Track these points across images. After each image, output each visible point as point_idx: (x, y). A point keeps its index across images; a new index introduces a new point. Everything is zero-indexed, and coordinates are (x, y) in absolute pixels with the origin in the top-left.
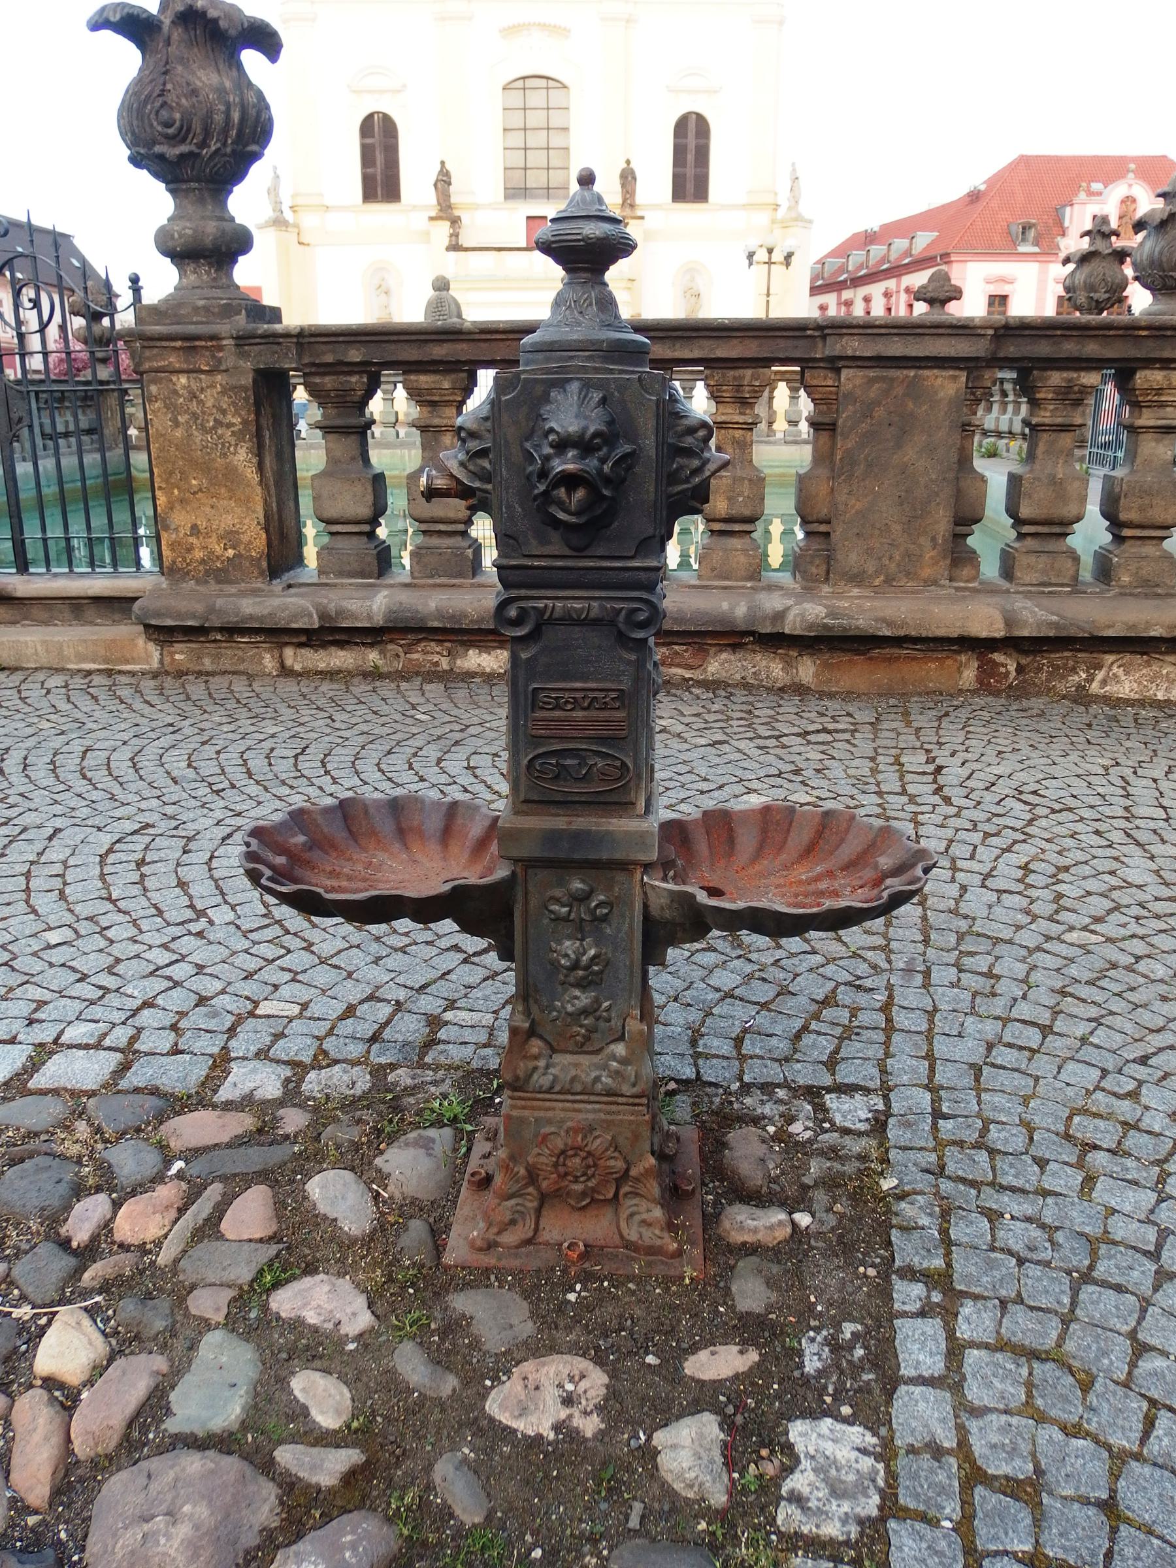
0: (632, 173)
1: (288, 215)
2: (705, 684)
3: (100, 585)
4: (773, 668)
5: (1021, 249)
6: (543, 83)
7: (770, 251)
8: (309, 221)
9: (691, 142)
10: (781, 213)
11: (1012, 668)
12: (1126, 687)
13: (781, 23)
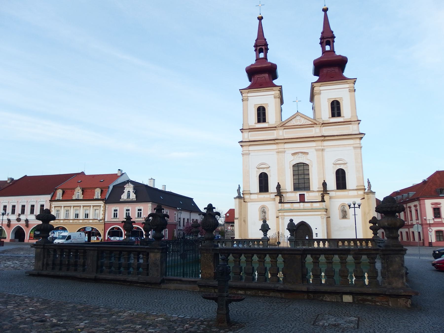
0: (326, 183)
1: (242, 195)
2: (269, 297)
3: (193, 279)
4: (279, 295)
5: (441, 196)
6: (302, 164)
7: (354, 205)
8: (247, 197)
9: (341, 175)
10: (366, 191)
11: (312, 296)
12: (328, 299)
13: (361, 148)
